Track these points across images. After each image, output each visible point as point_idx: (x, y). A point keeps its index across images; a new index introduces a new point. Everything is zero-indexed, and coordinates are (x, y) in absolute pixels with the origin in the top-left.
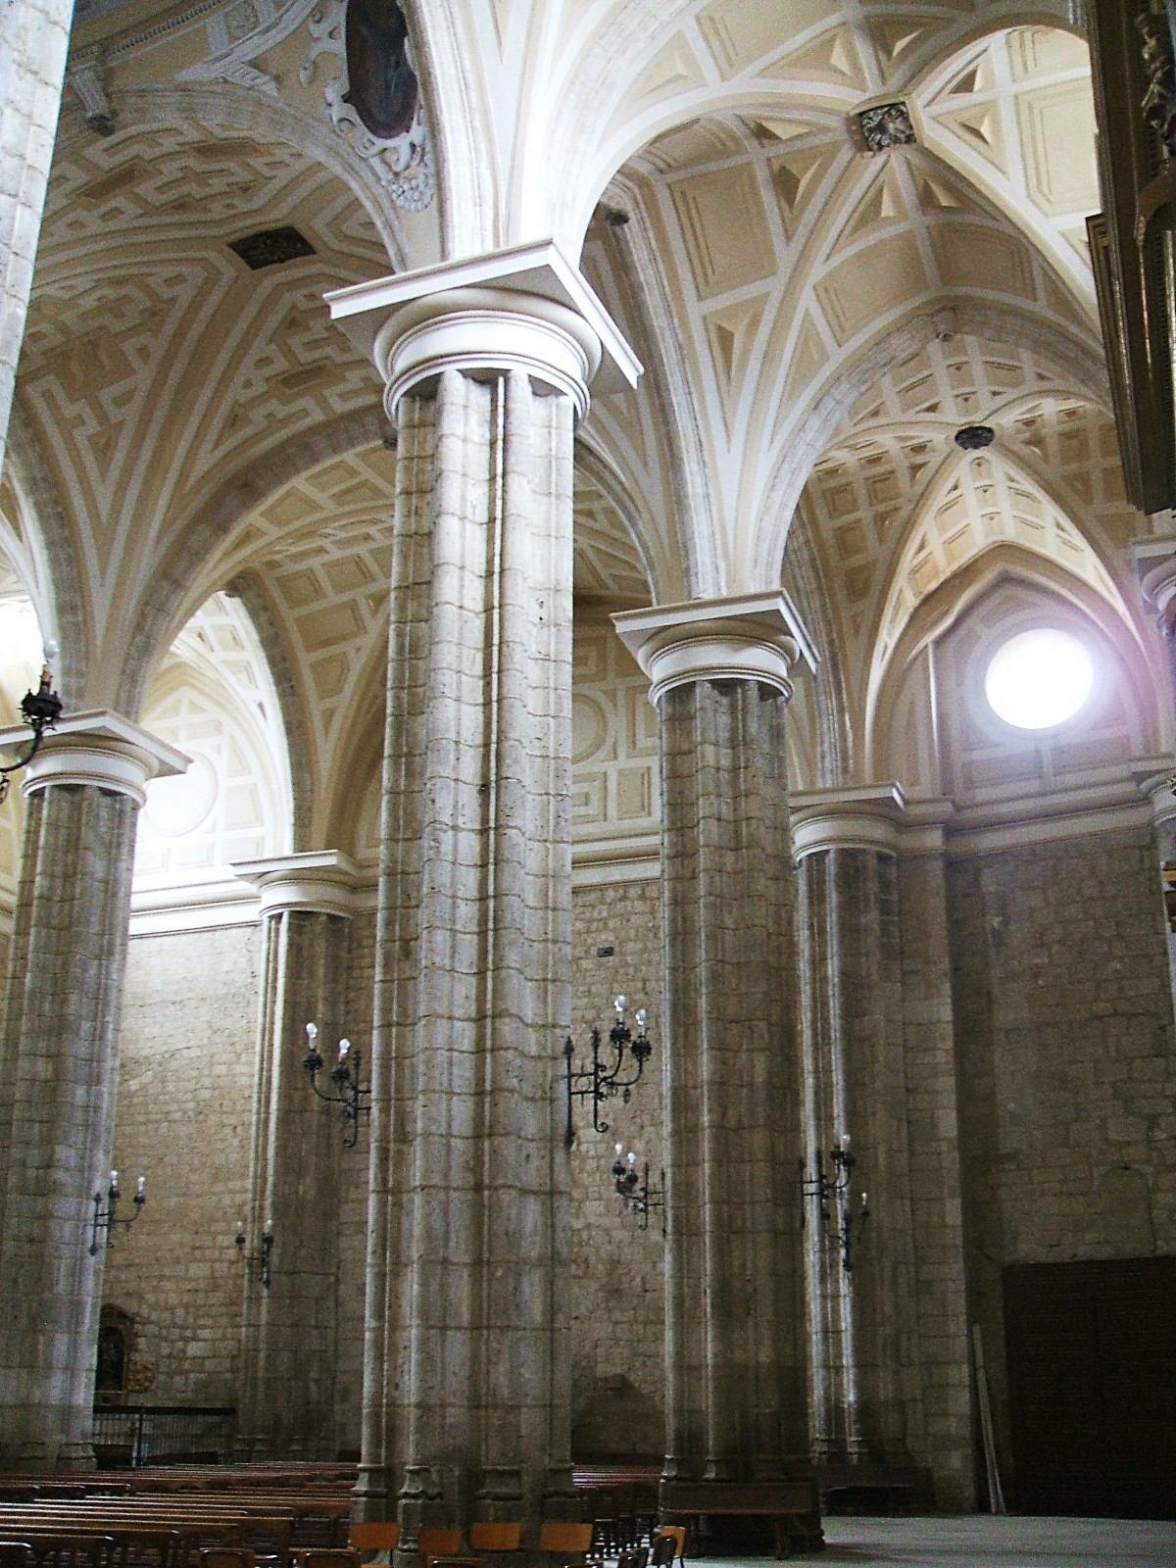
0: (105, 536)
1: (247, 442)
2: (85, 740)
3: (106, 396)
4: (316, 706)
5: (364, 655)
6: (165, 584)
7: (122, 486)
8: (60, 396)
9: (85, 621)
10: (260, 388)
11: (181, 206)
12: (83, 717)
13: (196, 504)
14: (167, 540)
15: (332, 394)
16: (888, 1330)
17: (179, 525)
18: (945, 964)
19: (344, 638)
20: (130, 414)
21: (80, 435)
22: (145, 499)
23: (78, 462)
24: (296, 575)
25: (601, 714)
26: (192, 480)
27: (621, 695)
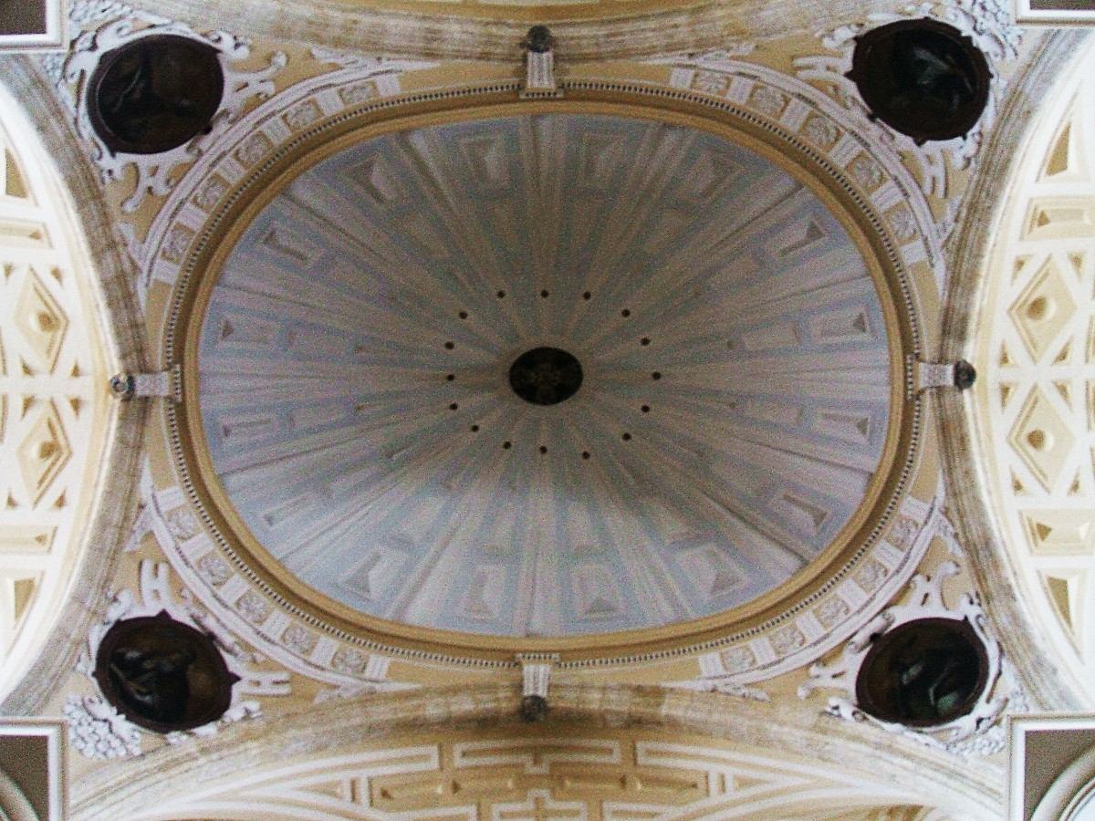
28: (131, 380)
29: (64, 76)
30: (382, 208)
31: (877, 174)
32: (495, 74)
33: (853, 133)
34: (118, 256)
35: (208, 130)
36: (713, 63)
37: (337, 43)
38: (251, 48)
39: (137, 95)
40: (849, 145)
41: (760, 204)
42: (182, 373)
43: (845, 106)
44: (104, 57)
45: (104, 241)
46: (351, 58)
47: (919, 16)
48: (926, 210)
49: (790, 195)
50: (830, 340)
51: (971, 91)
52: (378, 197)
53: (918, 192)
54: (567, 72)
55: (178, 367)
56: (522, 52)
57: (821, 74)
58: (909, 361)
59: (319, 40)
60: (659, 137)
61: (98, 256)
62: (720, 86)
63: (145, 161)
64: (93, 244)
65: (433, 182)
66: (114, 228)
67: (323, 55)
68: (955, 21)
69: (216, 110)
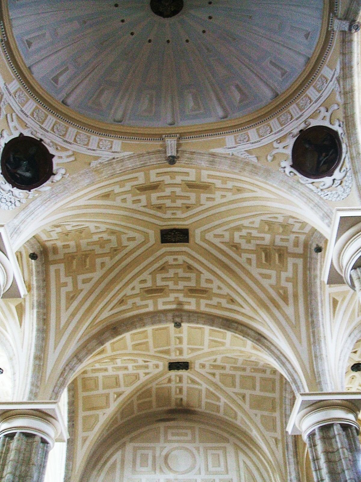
0: (60, 333)
1: (124, 311)
2: (41, 414)
3: (80, 278)
4: (80, 433)
5: (106, 417)
6: (75, 359)
7: (73, 315)
8: (62, 273)
9: (43, 364)
10: (137, 291)
11: (159, 208)
12: (43, 403)
13: (95, 331)
14: (81, 342)
17: (87, 337)
19: (101, 408)
20: (88, 287)
21: (64, 291)
22: (81, 322)
23: (58, 301)
24: (91, 378)
25: (193, 456)
26: (99, 320)
27: (201, 450)
28: (350, 30)
29: (347, 172)
30: (237, 82)
31: (35, 116)
32: (189, 144)
33: (48, 132)
34: (344, 88)
35: (301, 131)
36: (106, 155)
37: (247, 164)
38: (279, 165)
39: (324, 154)
40: (47, 126)
41: (78, 91)
42: (328, 26)
43: (52, 142)
44: (331, 175)
45: (348, 95)
46: (243, 156)
47: (33, 190)
48: (13, 107)
49: (68, 95)
50: (40, 33)
51: (7, 165)
52: (237, 86)
53: (17, 113)
54: (161, 146)
55: (330, 29)
56: (178, 155)
57: (64, 154)
58: (5, 38)
59: (254, 166)
60: (124, 116)
61: (352, 91)
62: (102, 143)
63: (326, 124)
64: (352, 97)
65: (214, 91)
66: (343, 101)
67: (253, 159)
68: (20, 193)
69: (297, 138)
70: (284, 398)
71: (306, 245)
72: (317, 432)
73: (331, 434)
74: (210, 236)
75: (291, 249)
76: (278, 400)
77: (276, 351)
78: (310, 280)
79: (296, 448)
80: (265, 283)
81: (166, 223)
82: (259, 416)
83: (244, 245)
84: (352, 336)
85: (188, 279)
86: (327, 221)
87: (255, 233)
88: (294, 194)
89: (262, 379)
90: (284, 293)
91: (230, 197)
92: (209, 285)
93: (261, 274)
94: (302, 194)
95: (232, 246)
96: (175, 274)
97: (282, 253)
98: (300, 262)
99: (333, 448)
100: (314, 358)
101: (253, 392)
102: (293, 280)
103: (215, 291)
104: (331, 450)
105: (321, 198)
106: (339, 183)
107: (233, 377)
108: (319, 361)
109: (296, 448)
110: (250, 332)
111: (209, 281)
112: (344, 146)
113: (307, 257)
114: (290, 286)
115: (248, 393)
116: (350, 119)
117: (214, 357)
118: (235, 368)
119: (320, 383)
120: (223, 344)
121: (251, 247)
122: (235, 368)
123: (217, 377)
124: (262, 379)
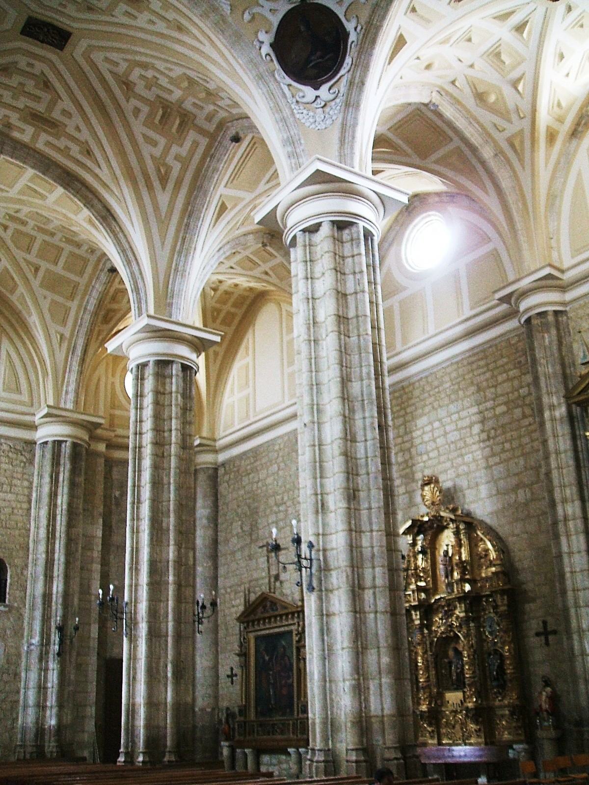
15: (44, 137)
16: (71, 688)
18: (101, 509)
38: (256, 33)
39: (319, 53)
63: (340, 12)
70: (91, 287)
71: (221, 125)
72: (151, 364)
73: (167, 372)
74: (98, 57)
75: (201, 121)
76: (82, 288)
77: (123, 241)
78: (207, 170)
79: (84, 355)
80: (147, 150)
81: (40, 11)
82: (49, 300)
83: (140, 89)
84: (222, 251)
85: (37, 99)
86: (290, 149)
87: (164, 81)
88: (261, 89)
89: (72, 254)
90: (166, 173)
91: (161, 27)
92: (66, 121)
93: (144, 135)
94: (271, 96)
95: (124, 83)
96: (20, 84)
97: (186, 120)
98: (204, 142)
99: (165, 389)
100: (173, 271)
101: (52, 268)
102: (185, 163)
103: (71, 130)
104: (162, 390)
105: (293, 114)
106: (322, 105)
107: (33, 239)
108: (179, 277)
109: (84, 355)
110: (96, 201)
111: (66, 113)
112: (348, 60)
113: (216, 141)
114: (177, 167)
115: (44, 265)
116: (373, 30)
117: (18, 207)
118: (40, 229)
119: (171, 305)
120: (43, 197)
121: (149, 95)
122: (40, 229)
123: (10, 232)
124: (72, 254)
